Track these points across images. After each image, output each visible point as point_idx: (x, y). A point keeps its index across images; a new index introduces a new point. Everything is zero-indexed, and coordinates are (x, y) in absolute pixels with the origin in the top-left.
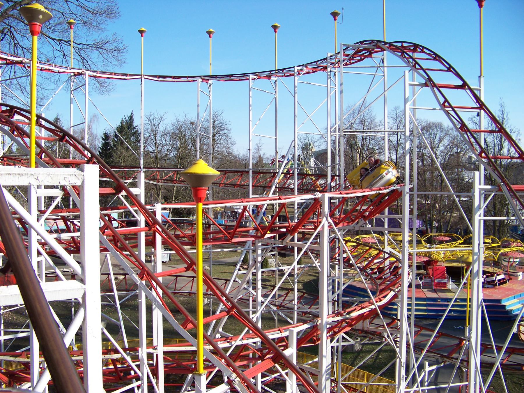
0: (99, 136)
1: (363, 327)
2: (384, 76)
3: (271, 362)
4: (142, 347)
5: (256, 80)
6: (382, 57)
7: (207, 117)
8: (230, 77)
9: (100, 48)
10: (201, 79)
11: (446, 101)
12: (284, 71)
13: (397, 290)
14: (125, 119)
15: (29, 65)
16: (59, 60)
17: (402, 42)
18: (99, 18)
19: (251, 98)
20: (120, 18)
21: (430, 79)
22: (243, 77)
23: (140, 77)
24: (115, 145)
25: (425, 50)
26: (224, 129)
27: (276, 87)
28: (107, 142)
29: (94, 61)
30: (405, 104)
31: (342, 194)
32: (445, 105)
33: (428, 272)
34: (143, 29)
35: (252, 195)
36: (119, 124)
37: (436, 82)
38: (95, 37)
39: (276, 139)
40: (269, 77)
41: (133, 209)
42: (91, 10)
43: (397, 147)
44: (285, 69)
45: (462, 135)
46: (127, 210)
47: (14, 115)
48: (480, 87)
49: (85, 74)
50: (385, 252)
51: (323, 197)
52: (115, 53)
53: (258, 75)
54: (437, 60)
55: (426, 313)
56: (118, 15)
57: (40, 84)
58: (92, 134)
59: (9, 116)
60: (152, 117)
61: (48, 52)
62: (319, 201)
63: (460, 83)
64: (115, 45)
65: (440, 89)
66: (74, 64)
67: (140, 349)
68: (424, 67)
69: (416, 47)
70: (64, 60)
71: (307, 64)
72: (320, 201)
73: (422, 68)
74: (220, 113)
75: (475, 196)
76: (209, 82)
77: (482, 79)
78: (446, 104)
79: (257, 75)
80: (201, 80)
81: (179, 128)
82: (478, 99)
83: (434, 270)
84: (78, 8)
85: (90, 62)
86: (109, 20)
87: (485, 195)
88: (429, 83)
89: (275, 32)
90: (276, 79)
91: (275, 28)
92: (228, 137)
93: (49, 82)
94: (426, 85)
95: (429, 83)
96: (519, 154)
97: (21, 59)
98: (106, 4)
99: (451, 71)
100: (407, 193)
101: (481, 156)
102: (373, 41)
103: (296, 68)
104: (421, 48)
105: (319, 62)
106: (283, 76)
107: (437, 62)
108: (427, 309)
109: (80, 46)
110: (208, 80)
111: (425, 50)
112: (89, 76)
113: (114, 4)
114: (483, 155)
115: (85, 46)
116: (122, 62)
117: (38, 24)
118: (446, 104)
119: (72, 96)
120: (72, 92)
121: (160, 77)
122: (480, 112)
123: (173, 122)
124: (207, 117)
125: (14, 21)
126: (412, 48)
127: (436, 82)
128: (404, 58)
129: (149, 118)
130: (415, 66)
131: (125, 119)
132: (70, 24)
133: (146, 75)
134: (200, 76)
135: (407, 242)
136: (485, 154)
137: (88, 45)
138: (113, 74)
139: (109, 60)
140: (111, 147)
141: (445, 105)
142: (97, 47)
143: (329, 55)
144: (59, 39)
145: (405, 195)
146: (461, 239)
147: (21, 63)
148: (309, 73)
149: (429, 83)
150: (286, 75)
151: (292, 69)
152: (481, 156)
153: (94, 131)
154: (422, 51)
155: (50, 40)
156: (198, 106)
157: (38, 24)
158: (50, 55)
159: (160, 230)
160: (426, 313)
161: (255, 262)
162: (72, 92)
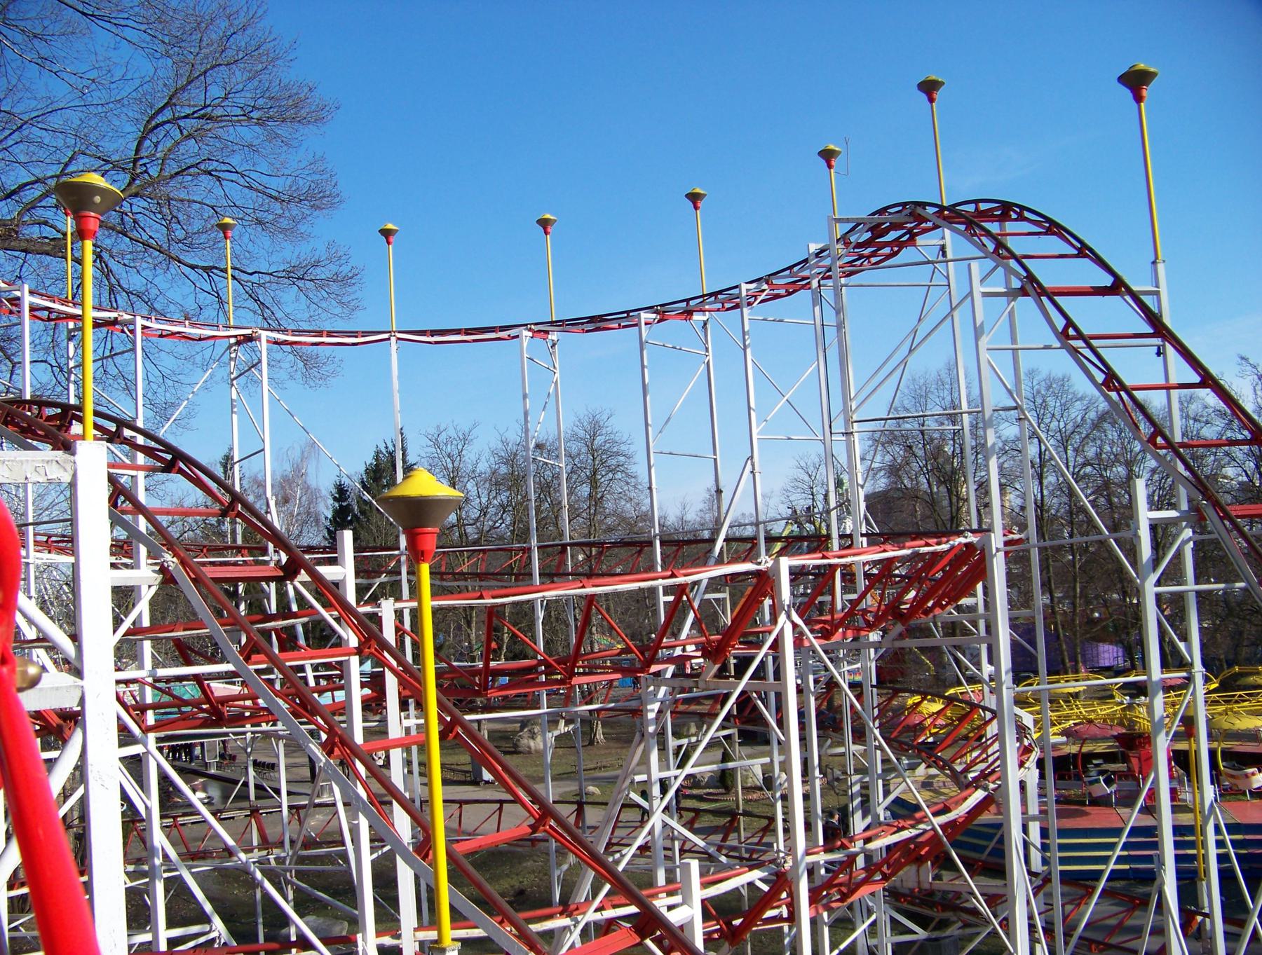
0: (324, 492)
1: (919, 883)
2: (949, 286)
3: (633, 934)
4: (364, 930)
5: (655, 326)
6: (941, 243)
7: (575, 428)
8: (597, 323)
9: (299, 278)
10: (530, 330)
11: (1070, 323)
12: (720, 297)
13: (992, 786)
14: (387, 448)
15: (131, 327)
16: (210, 314)
17: (976, 202)
18: (295, 210)
19: (646, 370)
20: (342, 206)
21: (1031, 278)
22: (627, 318)
23: (386, 336)
24: (363, 512)
25: (1026, 214)
26: (617, 454)
27: (706, 336)
28: (345, 504)
29: (288, 310)
30: (977, 339)
31: (828, 558)
32: (1069, 333)
33: (1130, 765)
34: (390, 226)
35: (664, 595)
36: (370, 460)
37: (1046, 285)
38: (288, 253)
39: (715, 460)
40: (688, 313)
41: (331, 615)
42: (274, 194)
43: (1042, 466)
44: (720, 292)
45: (1107, 398)
46: (316, 617)
47: (71, 424)
48: (1157, 286)
49: (259, 339)
50: (985, 709)
51: (777, 566)
52: (334, 287)
53: (662, 312)
54: (1054, 234)
55: (1127, 867)
56: (337, 200)
57: (169, 372)
58: (308, 488)
59: (59, 428)
60: (443, 437)
61: (185, 297)
62: (769, 577)
63: (1107, 281)
64: (334, 268)
65: (1056, 298)
66: (240, 319)
67: (359, 936)
68: (1018, 252)
69: (1006, 210)
70: (221, 312)
71: (769, 275)
72: (771, 575)
73: (1013, 256)
74: (605, 417)
75: (1139, 537)
76: (550, 337)
77: (1161, 267)
78: (1071, 332)
79: (657, 312)
80: (530, 334)
81: (511, 460)
82: (1153, 319)
83: (1142, 759)
84: (247, 190)
85: (279, 315)
86: (315, 213)
87: (1194, 543)
88: (1029, 288)
89: (696, 208)
90: (705, 318)
91: (694, 198)
92: (628, 475)
93: (191, 367)
94: (1023, 292)
95: (1029, 288)
96: (1251, 432)
97: (113, 315)
98: (309, 178)
99: (1086, 256)
100: (998, 550)
101: (1155, 445)
102: (904, 204)
103: (744, 287)
104: (1018, 210)
105: (795, 269)
106: (718, 310)
107: (1054, 238)
108: (1129, 856)
109: (255, 278)
110: (547, 332)
111: (1026, 214)
112: (268, 341)
113: (324, 177)
114: (1159, 440)
115: (267, 278)
116: (352, 308)
117: (93, 214)
118: (1071, 332)
119: (234, 396)
120: (235, 382)
121: (434, 333)
122: (1164, 346)
123: (493, 446)
124: (575, 428)
125: (109, 236)
126: (999, 213)
127: (1047, 283)
128: (973, 235)
129: (437, 440)
130: (1001, 251)
131: (387, 448)
132: (224, 228)
133: (400, 332)
134: (526, 325)
135: (1006, 673)
136: (1164, 437)
137: (271, 274)
138: (325, 334)
139: (324, 305)
140: (355, 516)
141: (1069, 333)
142: (295, 275)
143: (813, 248)
144: (206, 264)
145: (992, 556)
146: (1211, 680)
147: (115, 322)
148: (777, 296)
149: (1032, 287)
150: (727, 305)
151: (735, 291)
152: (1155, 445)
153: (312, 481)
154: (1021, 218)
155: (187, 270)
156: (525, 396)
157: (93, 214)
158: (191, 305)
159: (394, 663)
160: (1127, 867)
161: (643, 735)
162: (235, 382)
